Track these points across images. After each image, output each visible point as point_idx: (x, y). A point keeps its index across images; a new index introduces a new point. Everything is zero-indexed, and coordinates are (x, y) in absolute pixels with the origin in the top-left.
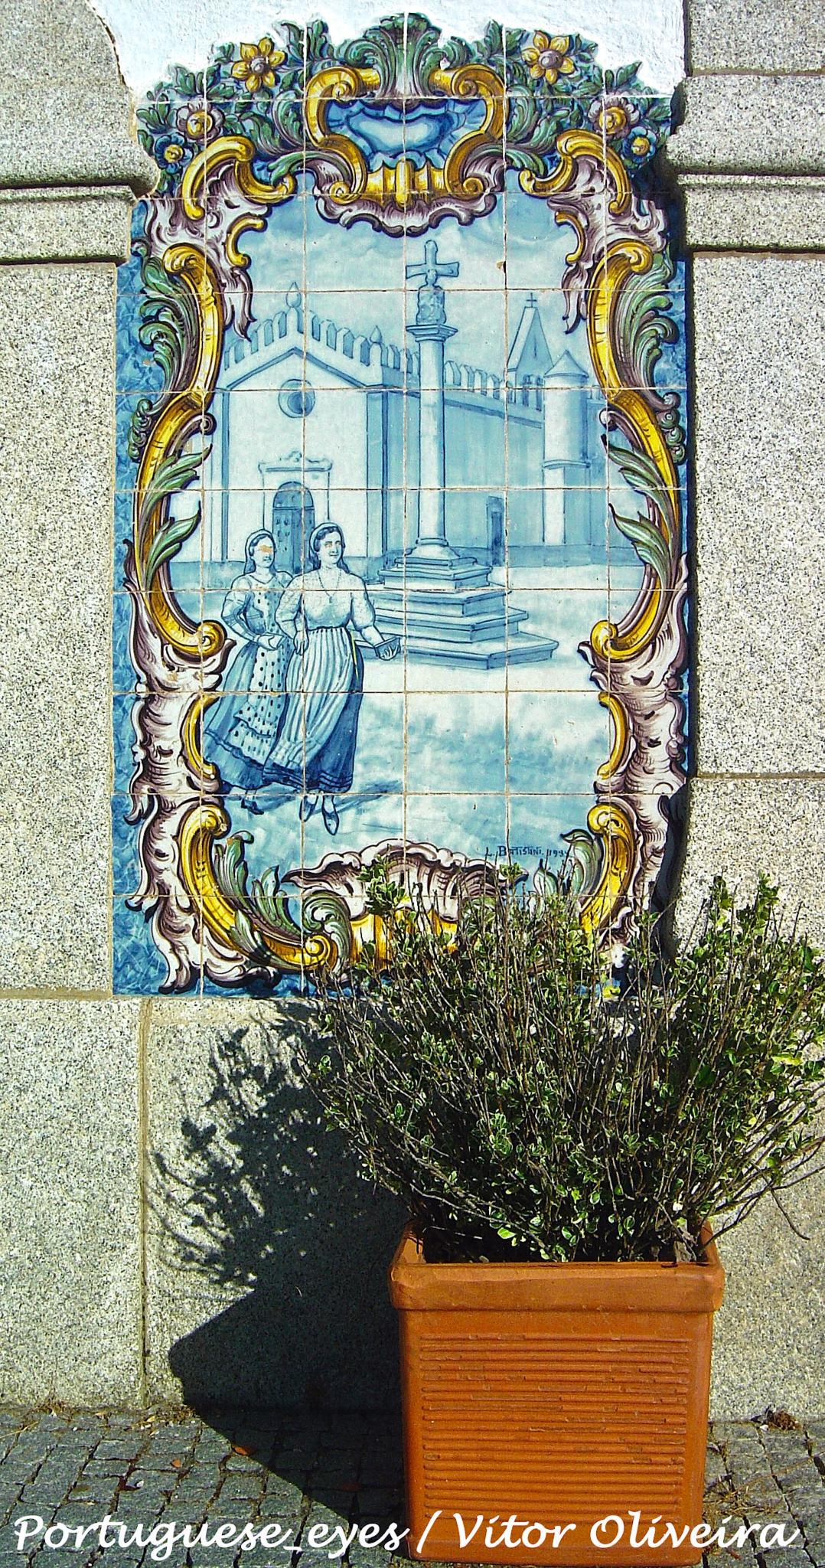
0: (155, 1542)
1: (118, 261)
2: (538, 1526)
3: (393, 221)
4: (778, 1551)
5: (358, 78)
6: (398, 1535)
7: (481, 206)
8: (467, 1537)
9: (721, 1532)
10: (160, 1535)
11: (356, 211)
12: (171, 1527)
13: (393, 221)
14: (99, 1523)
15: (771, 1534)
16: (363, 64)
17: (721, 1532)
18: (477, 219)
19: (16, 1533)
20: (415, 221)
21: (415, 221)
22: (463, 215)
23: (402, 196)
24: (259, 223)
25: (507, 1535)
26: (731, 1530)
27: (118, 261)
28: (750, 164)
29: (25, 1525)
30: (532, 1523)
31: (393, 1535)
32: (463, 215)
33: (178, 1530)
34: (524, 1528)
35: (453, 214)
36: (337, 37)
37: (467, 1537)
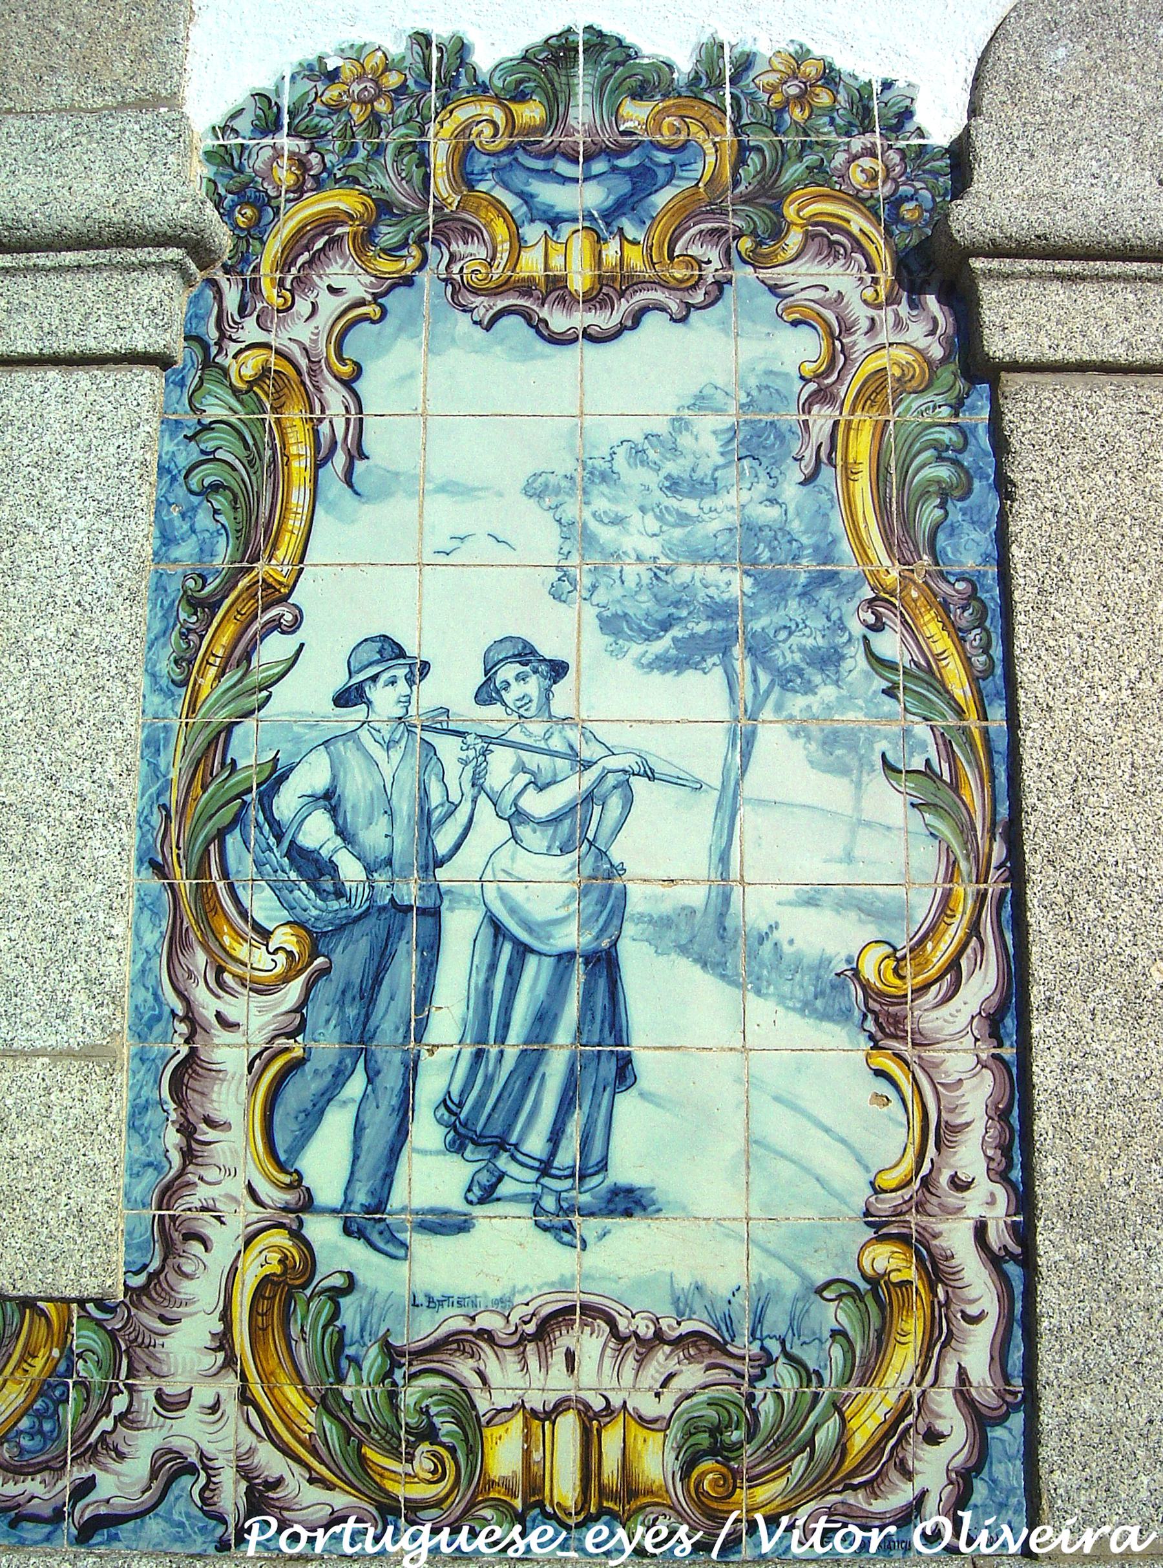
0: (408, 1547)
1: (162, 361)
2: (852, 1528)
3: (559, 321)
4: (1128, 1554)
5: (510, 116)
6: (690, 1538)
7: (698, 297)
8: (769, 1540)
9: (1065, 1535)
10: (414, 1538)
11: (501, 304)
12: (426, 1529)
13: (559, 321)
14: (342, 1525)
15: (1125, 1536)
16: (521, 97)
17: (1065, 1535)
18: (626, 332)
19: (246, 1536)
20: (603, 320)
21: (603, 320)
22: (674, 307)
23: (579, 282)
24: (371, 310)
25: (816, 1538)
26: (1076, 1531)
27: (162, 361)
28: (74, 226)
29: (256, 1527)
30: (845, 1525)
31: (684, 1539)
32: (674, 307)
33: (435, 1531)
34: (837, 1530)
35: (663, 309)
36: (484, 60)
37: (769, 1540)
